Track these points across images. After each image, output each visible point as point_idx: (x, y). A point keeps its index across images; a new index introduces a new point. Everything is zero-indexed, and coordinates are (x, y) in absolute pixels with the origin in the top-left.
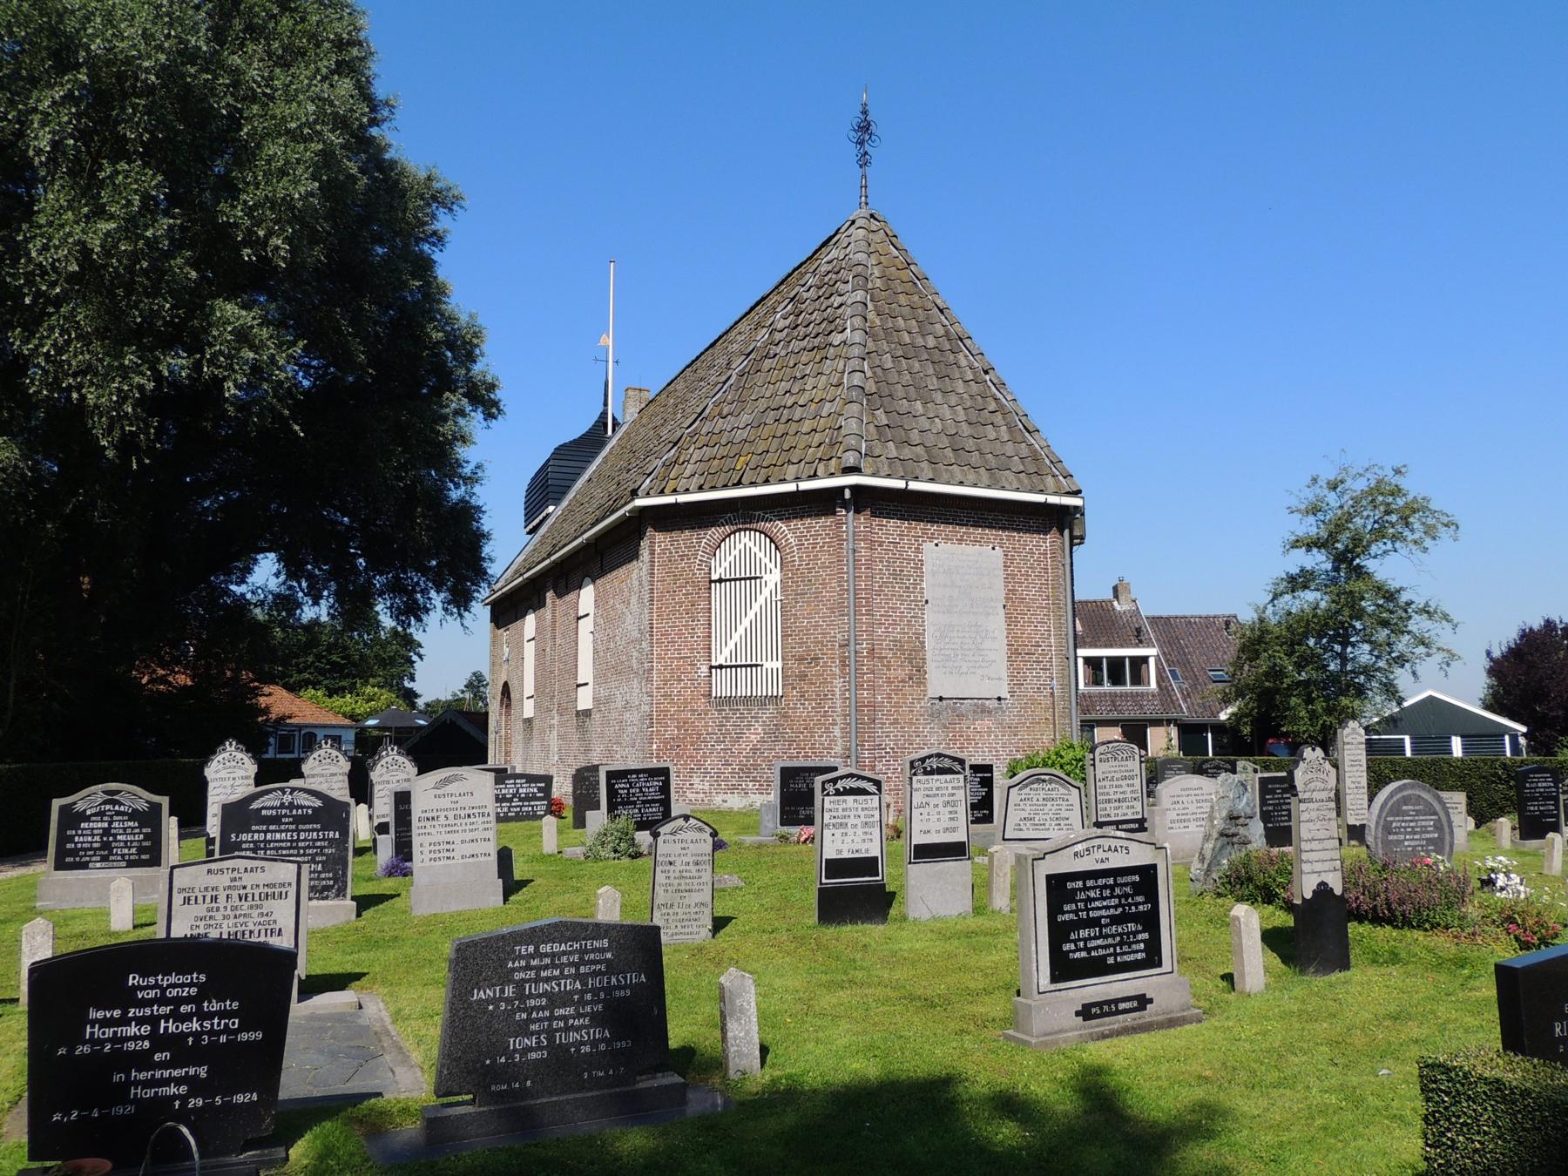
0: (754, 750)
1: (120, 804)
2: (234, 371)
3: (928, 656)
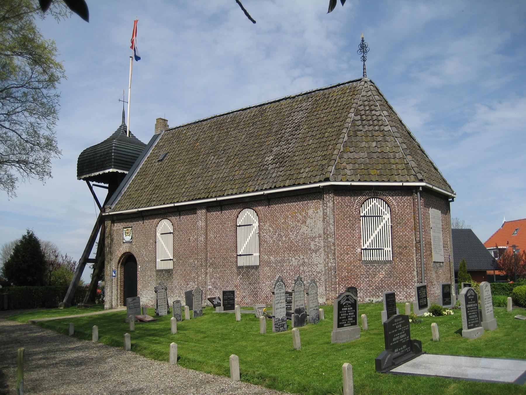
0: (382, 280)
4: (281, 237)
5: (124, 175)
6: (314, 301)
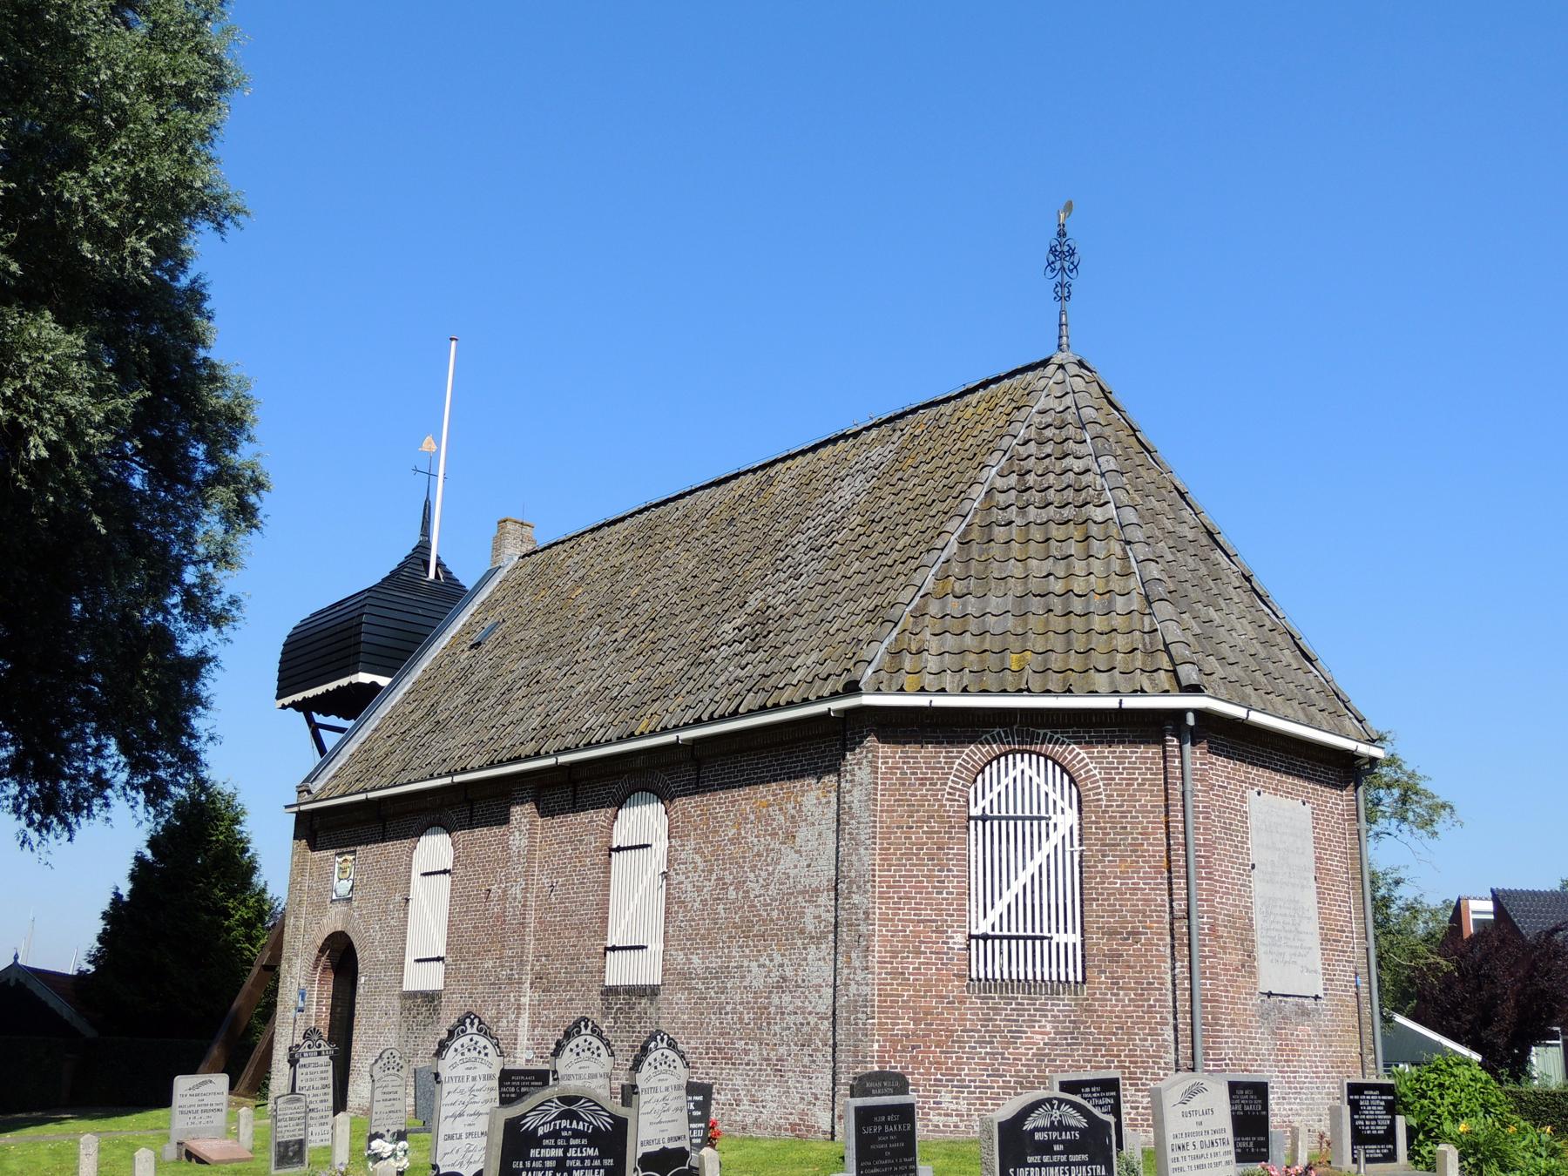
0: (1040, 1056)
1: (579, 1119)
2: (42, 421)
3: (1258, 937)
4: (725, 888)
5: (374, 687)
6: (664, 1117)
